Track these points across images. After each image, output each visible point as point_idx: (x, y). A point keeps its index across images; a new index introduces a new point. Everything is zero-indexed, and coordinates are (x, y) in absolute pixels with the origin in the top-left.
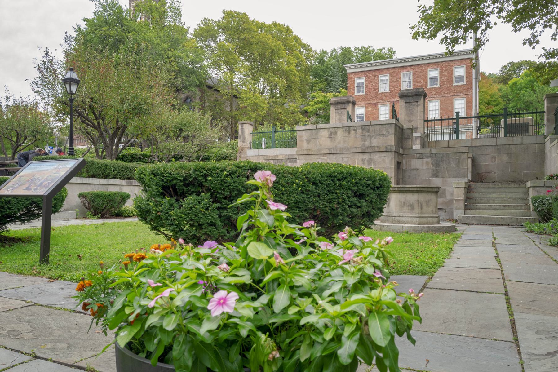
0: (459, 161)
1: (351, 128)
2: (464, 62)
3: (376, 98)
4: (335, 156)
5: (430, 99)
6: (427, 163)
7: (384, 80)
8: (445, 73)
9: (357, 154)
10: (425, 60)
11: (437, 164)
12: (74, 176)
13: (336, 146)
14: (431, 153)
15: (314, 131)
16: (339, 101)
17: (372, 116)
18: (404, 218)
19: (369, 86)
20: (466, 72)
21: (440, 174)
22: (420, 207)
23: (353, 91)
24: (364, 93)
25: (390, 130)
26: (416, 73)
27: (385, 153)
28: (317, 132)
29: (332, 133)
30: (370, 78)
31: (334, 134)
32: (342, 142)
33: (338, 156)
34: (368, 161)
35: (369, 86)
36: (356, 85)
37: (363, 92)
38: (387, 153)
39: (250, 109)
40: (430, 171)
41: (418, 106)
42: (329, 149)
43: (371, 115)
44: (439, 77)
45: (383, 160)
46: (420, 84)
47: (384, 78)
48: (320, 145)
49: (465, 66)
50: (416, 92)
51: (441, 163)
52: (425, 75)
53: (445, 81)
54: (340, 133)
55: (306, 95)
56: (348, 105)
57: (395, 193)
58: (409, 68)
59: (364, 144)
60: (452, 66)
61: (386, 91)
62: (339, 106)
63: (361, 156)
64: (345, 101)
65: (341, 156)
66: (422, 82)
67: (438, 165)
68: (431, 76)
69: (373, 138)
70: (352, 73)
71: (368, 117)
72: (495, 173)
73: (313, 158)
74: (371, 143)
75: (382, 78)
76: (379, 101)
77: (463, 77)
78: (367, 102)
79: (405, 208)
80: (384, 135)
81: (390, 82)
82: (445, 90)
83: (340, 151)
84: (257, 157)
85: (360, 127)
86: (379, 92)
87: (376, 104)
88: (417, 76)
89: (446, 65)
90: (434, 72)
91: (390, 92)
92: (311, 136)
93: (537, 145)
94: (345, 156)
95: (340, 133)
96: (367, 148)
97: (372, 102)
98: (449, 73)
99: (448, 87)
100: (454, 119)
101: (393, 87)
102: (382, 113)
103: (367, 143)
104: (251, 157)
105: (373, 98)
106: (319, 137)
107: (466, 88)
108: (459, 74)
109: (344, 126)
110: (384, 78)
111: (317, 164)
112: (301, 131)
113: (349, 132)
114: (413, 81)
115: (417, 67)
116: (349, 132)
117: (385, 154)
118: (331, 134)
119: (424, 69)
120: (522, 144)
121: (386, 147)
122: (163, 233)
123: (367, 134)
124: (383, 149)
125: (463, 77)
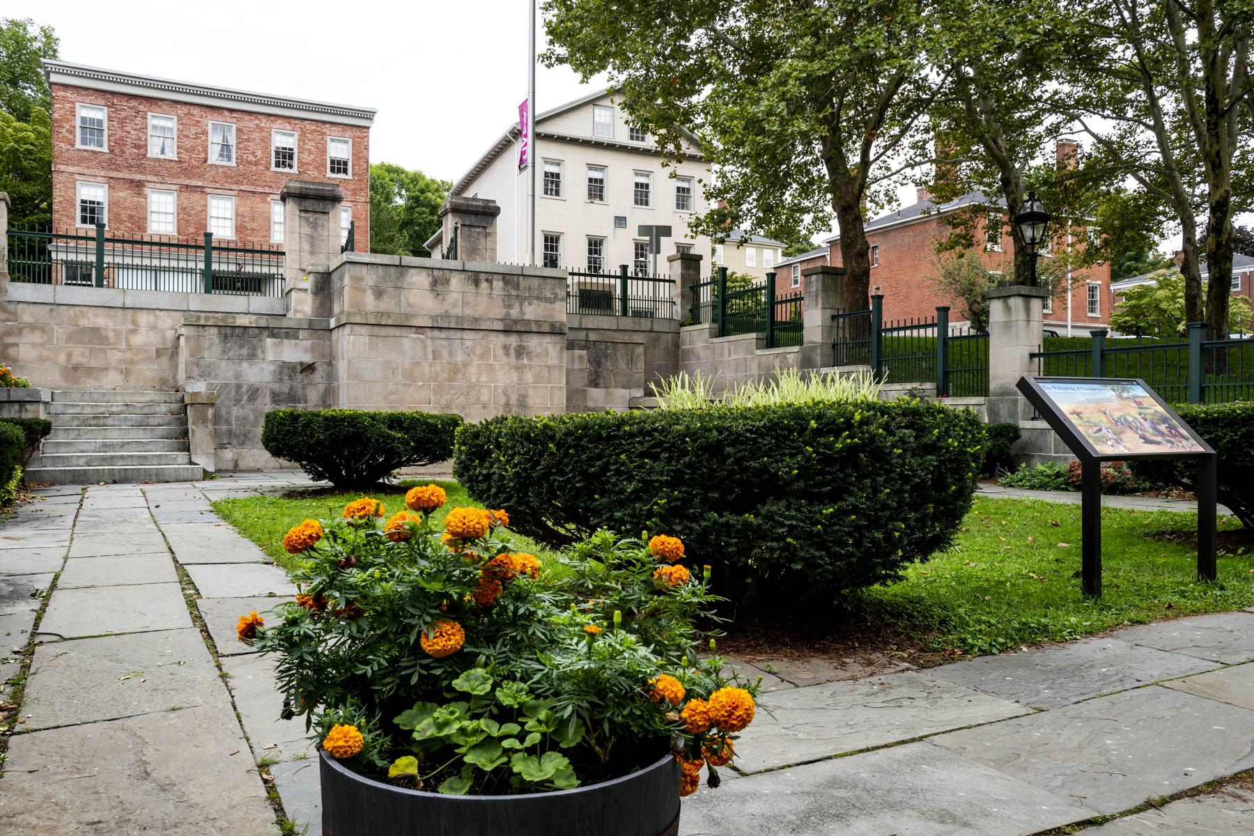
0: (632, 359)
1: (482, 275)
2: (350, 132)
3: (140, 168)
4: (443, 334)
6: (581, 357)
7: (163, 129)
8: (310, 145)
9: (494, 333)
10: (258, 103)
11: (596, 362)
13: (446, 311)
14: (587, 341)
15: (393, 270)
16: (312, 193)
17: (129, 212)
19: (119, 133)
20: (354, 154)
21: (601, 381)
24: (105, 149)
25: (558, 291)
26: (244, 130)
27: (549, 335)
28: (402, 275)
29: (438, 283)
30: (123, 114)
31: (442, 284)
32: (460, 303)
33: (452, 334)
34: (515, 349)
36: (78, 123)
38: (553, 337)
40: (586, 374)
41: (486, 237)
42: (432, 317)
43: (125, 208)
45: (546, 350)
46: (254, 159)
47: (162, 123)
48: (409, 305)
50: (484, 207)
51: (603, 361)
53: (308, 164)
54: (456, 282)
58: (226, 113)
59: (508, 314)
61: (162, 157)
62: (308, 204)
63: (501, 339)
64: (327, 194)
65: (459, 334)
66: (259, 153)
67: (599, 364)
69: (526, 303)
70: (66, 87)
71: (118, 214)
73: (391, 334)
74: (522, 313)
75: (155, 122)
76: (149, 178)
77: (345, 163)
78: (114, 174)
80: (547, 300)
81: (179, 137)
83: (457, 323)
84: (48, 307)
85: (501, 277)
86: (148, 155)
87: (138, 186)
89: (313, 128)
91: (180, 162)
92: (385, 281)
93: (670, 335)
94: (468, 335)
95: (456, 282)
96: (516, 322)
97: (127, 176)
98: (318, 148)
101: (186, 150)
102: (154, 209)
103: (514, 313)
104: (21, 306)
105: (132, 166)
106: (406, 286)
107: (353, 187)
110: (162, 123)
112: (358, 267)
113: (477, 283)
114: (238, 148)
115: (247, 117)
116: (477, 283)
117: (548, 339)
118: (435, 283)
119: (263, 125)
120: (651, 331)
121: (552, 325)
123: (514, 293)
124: (546, 328)
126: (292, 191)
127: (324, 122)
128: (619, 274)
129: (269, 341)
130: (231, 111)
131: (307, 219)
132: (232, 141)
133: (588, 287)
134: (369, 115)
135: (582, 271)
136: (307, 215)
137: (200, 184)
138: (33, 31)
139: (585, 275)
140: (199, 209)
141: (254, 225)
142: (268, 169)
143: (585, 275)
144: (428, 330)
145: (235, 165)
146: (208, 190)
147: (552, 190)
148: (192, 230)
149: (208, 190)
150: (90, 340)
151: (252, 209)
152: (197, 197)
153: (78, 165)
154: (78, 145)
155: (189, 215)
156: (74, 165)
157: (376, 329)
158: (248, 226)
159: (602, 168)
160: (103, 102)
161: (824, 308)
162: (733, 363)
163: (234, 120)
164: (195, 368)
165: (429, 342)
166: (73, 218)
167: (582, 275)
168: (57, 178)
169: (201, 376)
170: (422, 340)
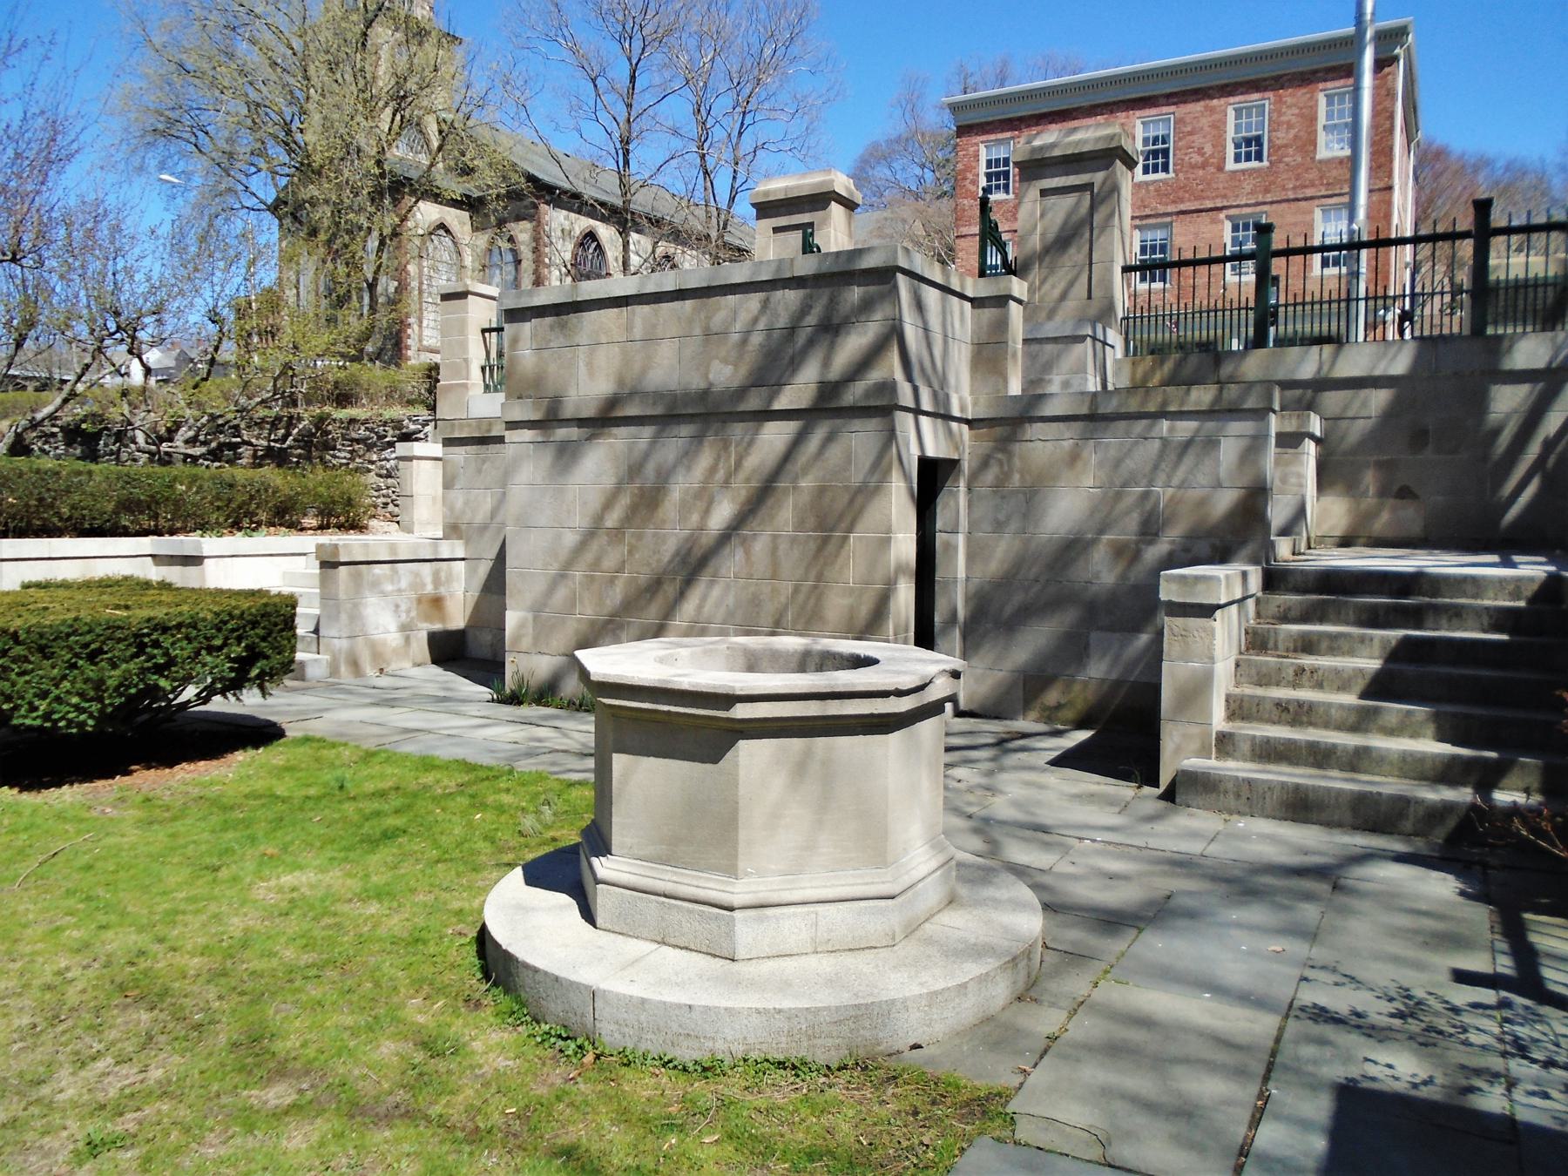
12: (1458, 875)
53: (1286, 146)
82: (1284, 176)
88: (1189, 129)
99: (1299, 166)
122: (1239, 925)
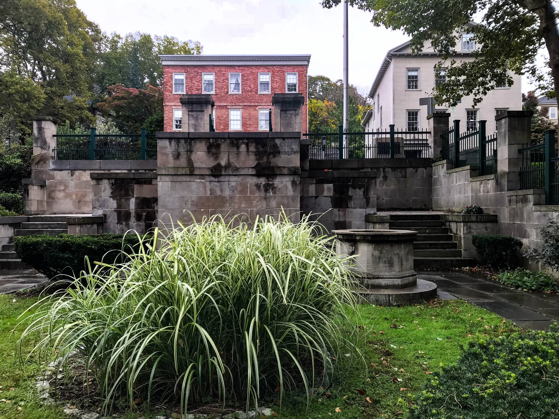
5: (260, 107)
8: (277, 79)
18: (380, 280)
19: (191, 84)
20: (299, 80)
22: (400, 263)
23: (170, 89)
26: (245, 75)
30: (192, 75)
35: (191, 84)
36: (174, 82)
37: (183, 91)
39: (17, 98)
41: (296, 116)
44: (270, 83)
46: (250, 89)
49: (297, 73)
52: (256, 79)
53: (276, 88)
55: (93, 88)
56: (206, 107)
57: (366, 244)
58: (237, 68)
60: (284, 72)
66: (252, 86)
68: (261, 80)
69: (271, 156)
70: (168, 66)
72: (383, 199)
77: (295, 86)
79: (381, 265)
89: (278, 69)
90: (264, 76)
91: (216, 95)
100: (388, 133)
101: (219, 88)
108: (291, 82)
109: (230, 137)
111: (481, 238)
114: (242, 85)
115: (246, 69)
125: (295, 86)
126: (184, 101)
127: (284, 66)
128: (389, 131)
129: (136, 187)
130: (239, 66)
131: (193, 116)
132: (240, 81)
133: (384, 141)
134: (307, 58)
135: (404, 131)
136: (192, 113)
137: (225, 104)
138: (191, 46)
139: (406, 133)
140: (225, 116)
141: (251, 122)
142: (257, 93)
143: (406, 133)
144: (207, 177)
145: (241, 93)
146: (229, 107)
147: (412, 86)
148: (222, 127)
149: (229, 107)
150: (85, 187)
151: (249, 114)
152: (224, 111)
153: (174, 102)
154: (173, 93)
155: (221, 120)
156: (172, 102)
157: (175, 177)
158: (248, 123)
159: (416, 70)
160: (183, 71)
161: (510, 144)
162: (458, 188)
163: (241, 71)
164: (97, 203)
165: (208, 183)
166: (172, 126)
167: (404, 133)
168: (166, 109)
169: (100, 207)
170: (203, 183)
